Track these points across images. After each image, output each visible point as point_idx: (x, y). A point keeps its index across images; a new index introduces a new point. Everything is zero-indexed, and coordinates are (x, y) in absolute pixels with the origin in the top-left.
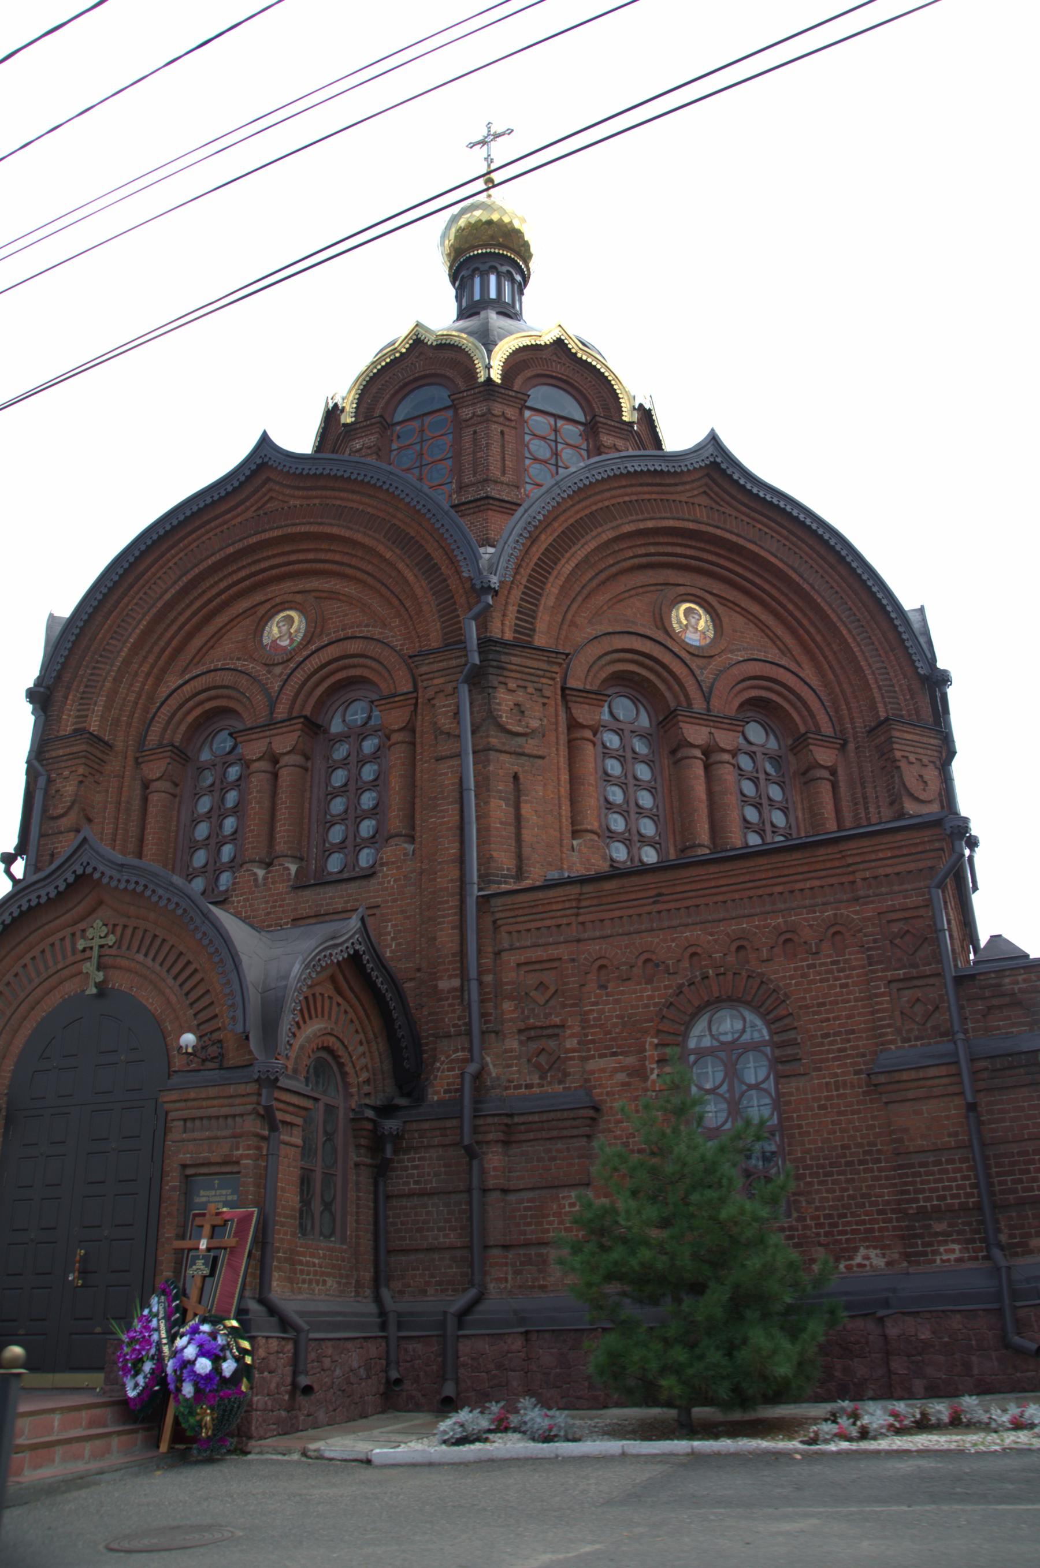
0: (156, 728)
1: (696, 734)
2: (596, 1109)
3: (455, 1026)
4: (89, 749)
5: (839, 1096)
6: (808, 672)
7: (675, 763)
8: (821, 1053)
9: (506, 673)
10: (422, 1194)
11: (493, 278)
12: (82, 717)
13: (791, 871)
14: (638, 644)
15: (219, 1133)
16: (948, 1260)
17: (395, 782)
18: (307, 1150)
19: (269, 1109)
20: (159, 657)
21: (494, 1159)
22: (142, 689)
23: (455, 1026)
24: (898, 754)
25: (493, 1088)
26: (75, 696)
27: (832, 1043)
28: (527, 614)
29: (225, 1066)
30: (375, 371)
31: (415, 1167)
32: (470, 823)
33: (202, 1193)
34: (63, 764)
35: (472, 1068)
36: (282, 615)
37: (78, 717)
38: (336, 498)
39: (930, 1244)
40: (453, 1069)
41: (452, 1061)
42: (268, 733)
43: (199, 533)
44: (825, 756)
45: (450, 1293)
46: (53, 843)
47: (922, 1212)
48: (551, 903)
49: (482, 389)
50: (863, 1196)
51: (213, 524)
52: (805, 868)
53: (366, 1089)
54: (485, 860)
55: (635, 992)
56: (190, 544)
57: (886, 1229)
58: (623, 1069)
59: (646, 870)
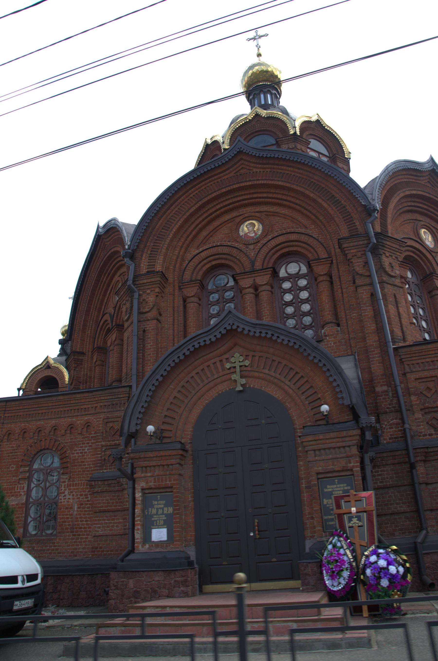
3: (388, 408)
4: (161, 280)
7: (431, 297)
9: (385, 249)
11: (262, 96)
15: (338, 456)
20: (186, 240)
21: (420, 469)
23: (388, 408)
26: (146, 255)
29: (330, 422)
30: (237, 126)
32: (384, 314)
34: (146, 287)
36: (251, 221)
37: (148, 265)
38: (279, 169)
40: (392, 428)
41: (391, 424)
42: (253, 275)
43: (206, 182)
45: (407, 534)
46: (144, 325)
48: (81, 399)
49: (292, 137)
51: (213, 178)
56: (201, 187)
59: (425, 342)
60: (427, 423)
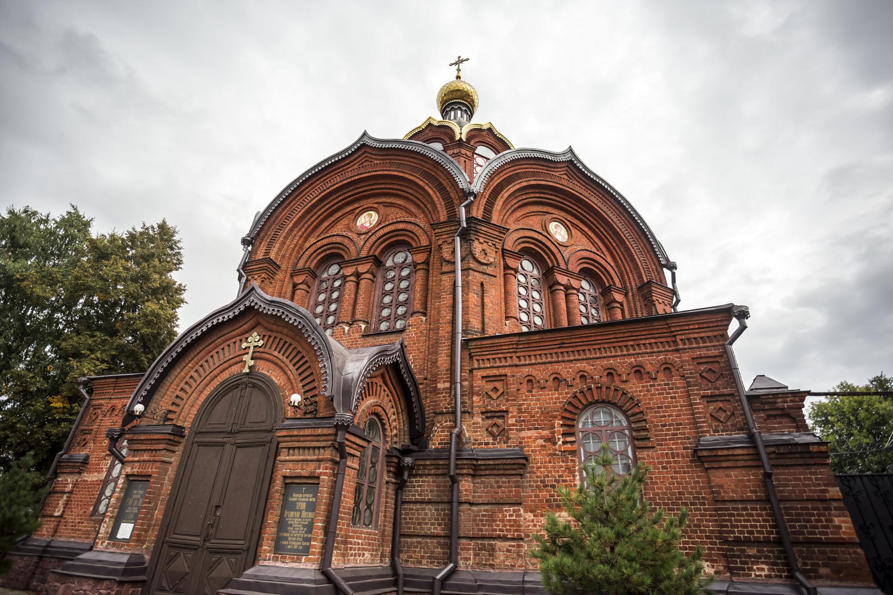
0: (302, 261)
1: (563, 279)
2: (527, 459)
3: (446, 408)
5: (674, 462)
6: (609, 259)
8: (661, 435)
10: (422, 502)
12: (267, 253)
13: (639, 334)
14: (536, 235)
16: (760, 576)
17: (418, 288)
18: (361, 472)
19: (341, 445)
21: (466, 485)
22: (297, 243)
23: (446, 408)
24: (654, 298)
25: (467, 443)
27: (668, 430)
28: (488, 210)
31: (419, 486)
33: (294, 495)
35: (456, 431)
39: (747, 563)
41: (443, 427)
44: (619, 297)
47: (737, 541)
50: (695, 526)
52: (647, 333)
53: (395, 439)
54: (466, 323)
55: (548, 395)
57: (713, 549)
58: (541, 438)
60: (487, 430)
